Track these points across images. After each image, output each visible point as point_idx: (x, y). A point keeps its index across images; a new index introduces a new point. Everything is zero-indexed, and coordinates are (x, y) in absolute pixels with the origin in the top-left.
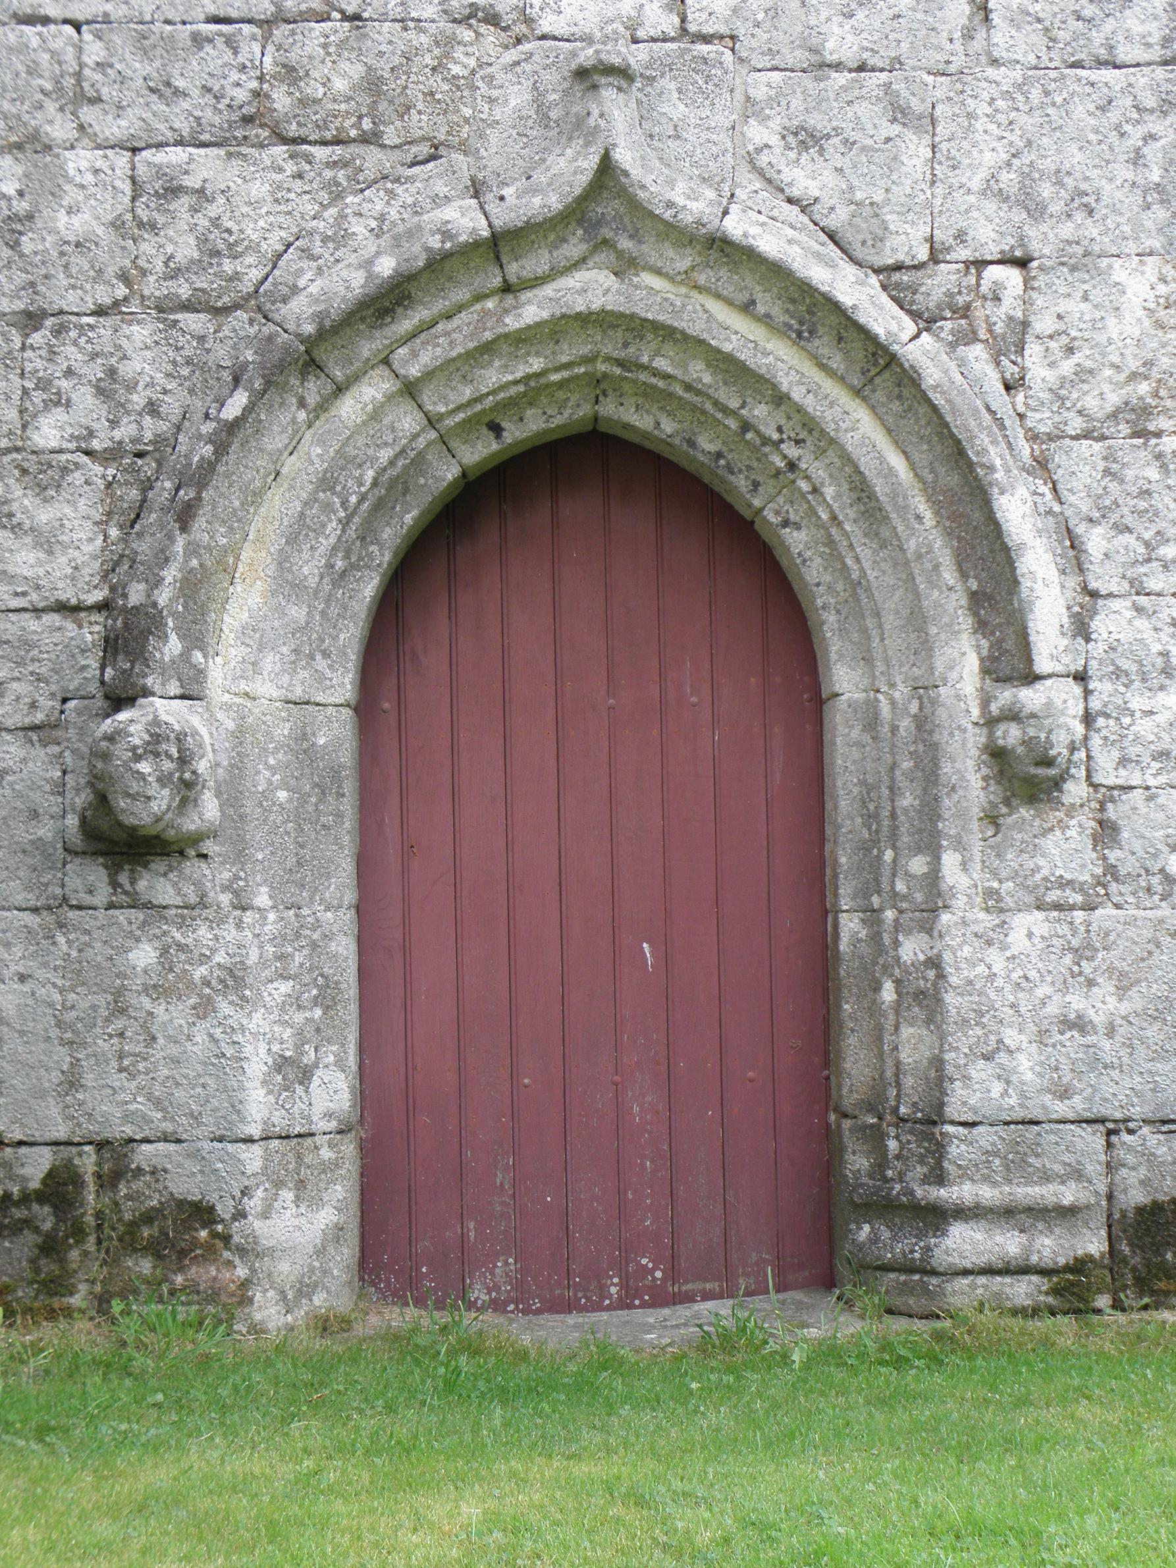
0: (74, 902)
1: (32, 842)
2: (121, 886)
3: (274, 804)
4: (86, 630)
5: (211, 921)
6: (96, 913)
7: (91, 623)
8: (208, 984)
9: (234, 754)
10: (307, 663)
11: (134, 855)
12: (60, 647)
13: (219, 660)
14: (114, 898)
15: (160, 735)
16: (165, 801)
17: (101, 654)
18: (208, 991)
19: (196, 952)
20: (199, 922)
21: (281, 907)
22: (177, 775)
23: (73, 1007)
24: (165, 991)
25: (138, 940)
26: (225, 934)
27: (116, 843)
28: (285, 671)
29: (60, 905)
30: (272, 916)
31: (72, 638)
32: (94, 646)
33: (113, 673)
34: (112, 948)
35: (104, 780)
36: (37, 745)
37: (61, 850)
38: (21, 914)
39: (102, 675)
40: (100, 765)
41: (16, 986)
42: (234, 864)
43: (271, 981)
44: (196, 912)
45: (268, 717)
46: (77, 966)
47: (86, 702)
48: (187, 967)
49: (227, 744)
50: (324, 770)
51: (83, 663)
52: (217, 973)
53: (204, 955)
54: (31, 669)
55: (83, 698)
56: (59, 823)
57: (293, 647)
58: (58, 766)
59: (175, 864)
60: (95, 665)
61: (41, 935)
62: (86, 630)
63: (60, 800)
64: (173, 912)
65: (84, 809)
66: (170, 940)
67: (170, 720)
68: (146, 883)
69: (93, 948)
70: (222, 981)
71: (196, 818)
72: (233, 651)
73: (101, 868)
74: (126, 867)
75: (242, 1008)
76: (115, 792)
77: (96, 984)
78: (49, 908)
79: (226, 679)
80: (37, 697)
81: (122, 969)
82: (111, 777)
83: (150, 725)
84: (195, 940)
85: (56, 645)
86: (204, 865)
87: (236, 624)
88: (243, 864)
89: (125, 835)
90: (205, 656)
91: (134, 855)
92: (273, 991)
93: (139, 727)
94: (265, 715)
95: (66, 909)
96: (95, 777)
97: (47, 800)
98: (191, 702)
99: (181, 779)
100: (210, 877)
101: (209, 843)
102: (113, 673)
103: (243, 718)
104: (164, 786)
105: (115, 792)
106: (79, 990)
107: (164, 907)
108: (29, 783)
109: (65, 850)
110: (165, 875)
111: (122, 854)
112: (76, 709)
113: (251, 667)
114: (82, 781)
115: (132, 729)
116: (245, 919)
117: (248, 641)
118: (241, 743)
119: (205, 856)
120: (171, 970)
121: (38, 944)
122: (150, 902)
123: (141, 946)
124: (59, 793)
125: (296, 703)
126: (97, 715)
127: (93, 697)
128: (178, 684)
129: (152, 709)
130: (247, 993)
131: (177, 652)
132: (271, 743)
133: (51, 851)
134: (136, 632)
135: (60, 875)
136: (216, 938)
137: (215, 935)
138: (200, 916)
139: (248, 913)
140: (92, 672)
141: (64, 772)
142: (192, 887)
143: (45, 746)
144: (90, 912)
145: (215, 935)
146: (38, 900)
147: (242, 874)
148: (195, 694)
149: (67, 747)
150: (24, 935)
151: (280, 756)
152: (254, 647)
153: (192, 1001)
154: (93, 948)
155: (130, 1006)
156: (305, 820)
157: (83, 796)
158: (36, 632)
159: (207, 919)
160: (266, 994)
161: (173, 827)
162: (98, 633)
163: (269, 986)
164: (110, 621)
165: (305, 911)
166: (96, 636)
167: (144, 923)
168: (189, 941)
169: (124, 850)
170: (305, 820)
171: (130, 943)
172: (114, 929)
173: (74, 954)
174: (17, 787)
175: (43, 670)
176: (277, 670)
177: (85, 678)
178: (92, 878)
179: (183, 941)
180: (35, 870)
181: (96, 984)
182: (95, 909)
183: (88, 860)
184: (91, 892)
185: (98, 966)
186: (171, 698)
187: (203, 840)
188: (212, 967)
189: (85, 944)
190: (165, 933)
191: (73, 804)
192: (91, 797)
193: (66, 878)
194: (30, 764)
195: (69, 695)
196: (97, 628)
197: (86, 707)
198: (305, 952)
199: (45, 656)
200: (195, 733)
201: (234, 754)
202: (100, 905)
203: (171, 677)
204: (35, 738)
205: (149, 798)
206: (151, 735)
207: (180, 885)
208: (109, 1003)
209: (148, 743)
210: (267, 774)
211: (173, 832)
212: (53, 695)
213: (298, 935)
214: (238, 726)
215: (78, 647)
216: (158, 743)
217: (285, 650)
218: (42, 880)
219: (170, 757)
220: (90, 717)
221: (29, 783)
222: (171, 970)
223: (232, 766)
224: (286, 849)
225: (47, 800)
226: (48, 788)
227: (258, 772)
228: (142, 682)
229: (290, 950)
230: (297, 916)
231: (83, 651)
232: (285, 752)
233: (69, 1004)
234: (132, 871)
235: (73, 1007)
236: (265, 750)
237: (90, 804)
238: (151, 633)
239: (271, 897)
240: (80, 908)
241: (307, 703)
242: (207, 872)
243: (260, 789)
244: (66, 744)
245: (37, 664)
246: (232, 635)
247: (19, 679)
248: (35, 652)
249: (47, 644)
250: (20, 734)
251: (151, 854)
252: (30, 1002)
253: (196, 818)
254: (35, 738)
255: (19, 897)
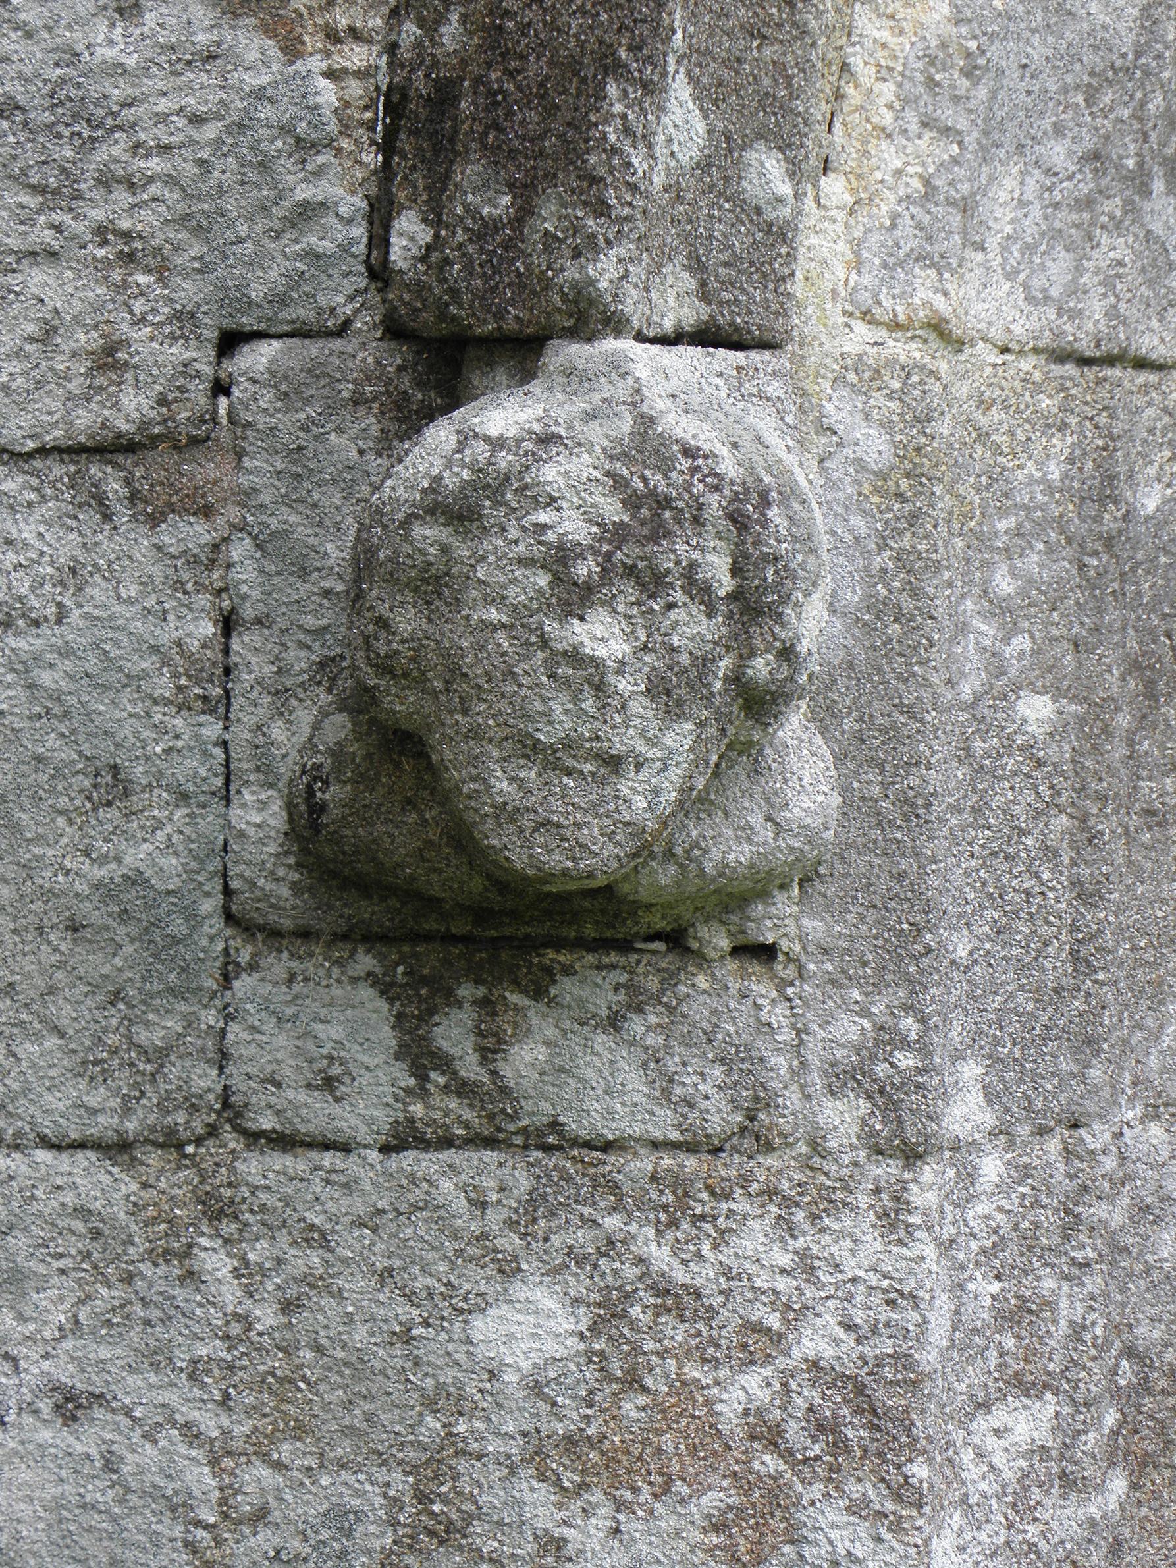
0: (267, 1123)
1: (105, 891)
2: (444, 1063)
3: (1007, 744)
4: (316, 63)
5: (789, 1203)
6: (350, 1164)
7: (333, 36)
8: (773, 1439)
9: (884, 560)
10: (1130, 207)
11: (495, 943)
12: (211, 131)
13: (835, 187)
14: (417, 1109)
15: (665, 502)
16: (675, 774)
17: (373, 159)
18: (770, 1463)
19: (729, 1320)
20: (740, 1205)
21: (1023, 1130)
22: (725, 664)
23: (260, 1516)
24: (610, 1461)
25: (509, 1270)
26: (840, 1250)
27: (431, 903)
28: (1055, 235)
29: (213, 1131)
30: (991, 1167)
31: (259, 94)
32: (346, 129)
33: (425, 235)
34: (410, 1297)
35: (422, 681)
36: (123, 515)
37: (216, 924)
38: (64, 1162)
39: (379, 239)
40: (407, 620)
41: (45, 1435)
42: (878, 987)
43: (984, 1406)
44: (728, 1167)
45: (996, 414)
46: (276, 1362)
47: (314, 348)
48: (693, 1372)
49: (858, 522)
50: (1152, 608)
51: (304, 193)
52: (807, 1394)
53: (758, 1328)
54: (98, 215)
55: (301, 332)
56: (209, 822)
57: (1089, 143)
58: (203, 600)
59: (652, 984)
60: (353, 203)
61: (142, 1245)
62: (316, 63)
63: (212, 729)
64: (643, 1164)
65: (316, 775)
66: (631, 1271)
67: (704, 436)
68: (542, 1053)
69: (339, 1295)
70: (822, 1427)
71: (756, 820)
72: (889, 156)
73: (366, 993)
74: (465, 991)
75: (897, 1527)
76: (475, 734)
77: (349, 1431)
78: (171, 1142)
79: (858, 264)
80: (125, 329)
81: (448, 1376)
82: (455, 673)
83: (625, 457)
84: (727, 1273)
85: (197, 120)
86: (762, 989)
87: (903, 45)
88: (914, 985)
89: (477, 884)
90: (794, 172)
91: (495, 943)
92: (991, 1442)
93: (583, 465)
94: (985, 405)
95: (233, 1142)
96: (385, 668)
97: (161, 730)
98: (739, 357)
99: (736, 679)
100: (787, 1035)
101: (784, 905)
102: (425, 235)
103: (923, 420)
104: (673, 711)
105: (475, 734)
106: (284, 1451)
107: (607, 1147)
108: (92, 663)
109: (229, 917)
110: (614, 1022)
111: (449, 939)
112: (275, 376)
113: (956, 219)
114: (300, 660)
115: (551, 474)
116: (917, 1198)
117: (948, 114)
118: (914, 518)
119: (766, 953)
120: (633, 1382)
121: (128, 1279)
122: (555, 1125)
123: (519, 1290)
124: (208, 705)
125: (1085, 362)
126: (357, 401)
127: (343, 330)
128: (690, 283)
129: (622, 390)
130: (919, 1471)
131: (689, 155)
132: (1003, 512)
133: (177, 926)
134: (536, 68)
135: (210, 1018)
136: (806, 1266)
137: (803, 1255)
138: (745, 1180)
139: (927, 1173)
140: (340, 233)
141: (228, 624)
142: (717, 1073)
143: (155, 521)
144: (328, 1159)
145: (803, 1255)
146: (127, 1111)
147: (909, 1025)
148: (755, 323)
149: (241, 527)
150: (75, 1246)
151: (1032, 562)
152: (971, 140)
153: (710, 1501)
154: (339, 1295)
155: (480, 1514)
156: (1102, 798)
157: (304, 717)
158: (120, 69)
159: (770, 1193)
160: (967, 1456)
161: (669, 855)
162: (359, 74)
163: (982, 1423)
164: (411, 30)
165: (1096, 1137)
166: (355, 89)
167: (533, 1201)
168: (704, 1275)
169: (459, 927)
170: (1102, 798)
171: (475, 1280)
172: (419, 1227)
173: (266, 1316)
174: (46, 678)
175: (148, 220)
176: (1030, 231)
177: (312, 255)
178: (335, 1032)
179: (680, 1275)
180: (116, 997)
181: (349, 1431)
182: (345, 1148)
183: (316, 964)
184: (329, 1084)
185: (358, 1365)
186: (653, 341)
187: (764, 895)
188: (786, 1377)
189: (307, 1280)
190: (610, 1246)
191: (261, 749)
192: (338, 727)
193: (235, 1031)
194: (97, 591)
195: (248, 322)
196: (357, 56)
197: (314, 371)
198: (1093, 1283)
199: (155, 164)
200: (789, 494)
201: (884, 560)
202: (363, 1134)
203: (666, 255)
204: (114, 487)
205: (614, 763)
206: (632, 502)
207: (671, 1065)
208: (395, 1503)
209: (618, 534)
210: (987, 630)
211: (666, 875)
212: (185, 318)
213: (1072, 1224)
214: (902, 451)
215: (286, 130)
216: (658, 533)
217: (1059, 153)
218: (142, 1036)
219: (701, 592)
220: (330, 410)
221: (92, 663)
222: (633, 1382)
223: (876, 607)
224: (1044, 914)
225: (161, 730)
226: (163, 685)
227: (963, 629)
228: (571, 272)
229: (1048, 1284)
230: (1068, 1153)
231: (304, 147)
232: (1050, 550)
233: (245, 1505)
234: (487, 1005)
235: (260, 1516)
236: (982, 540)
237: (337, 753)
238: (616, 68)
239: (991, 1096)
240: (285, 1141)
241: (1110, 360)
242: (778, 1015)
243: (966, 690)
244: (233, 513)
245: (122, 197)
246: (887, 91)
247: (53, 255)
248: (116, 148)
249: (162, 118)
250: (58, 470)
251: (559, 944)
252: (100, 1493)
253: (756, 820)
254: (114, 487)
255: (56, 1102)
